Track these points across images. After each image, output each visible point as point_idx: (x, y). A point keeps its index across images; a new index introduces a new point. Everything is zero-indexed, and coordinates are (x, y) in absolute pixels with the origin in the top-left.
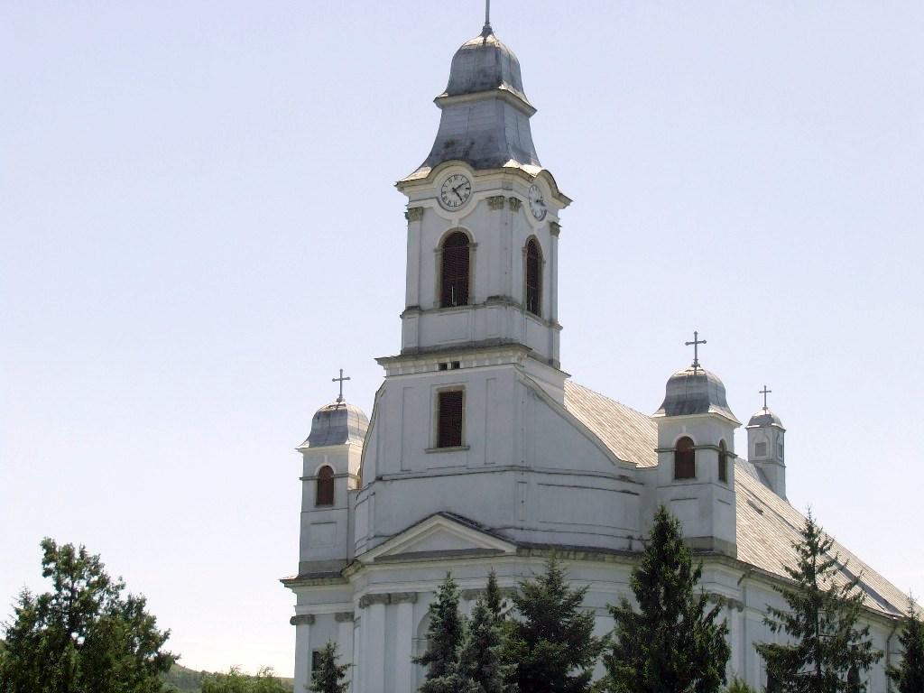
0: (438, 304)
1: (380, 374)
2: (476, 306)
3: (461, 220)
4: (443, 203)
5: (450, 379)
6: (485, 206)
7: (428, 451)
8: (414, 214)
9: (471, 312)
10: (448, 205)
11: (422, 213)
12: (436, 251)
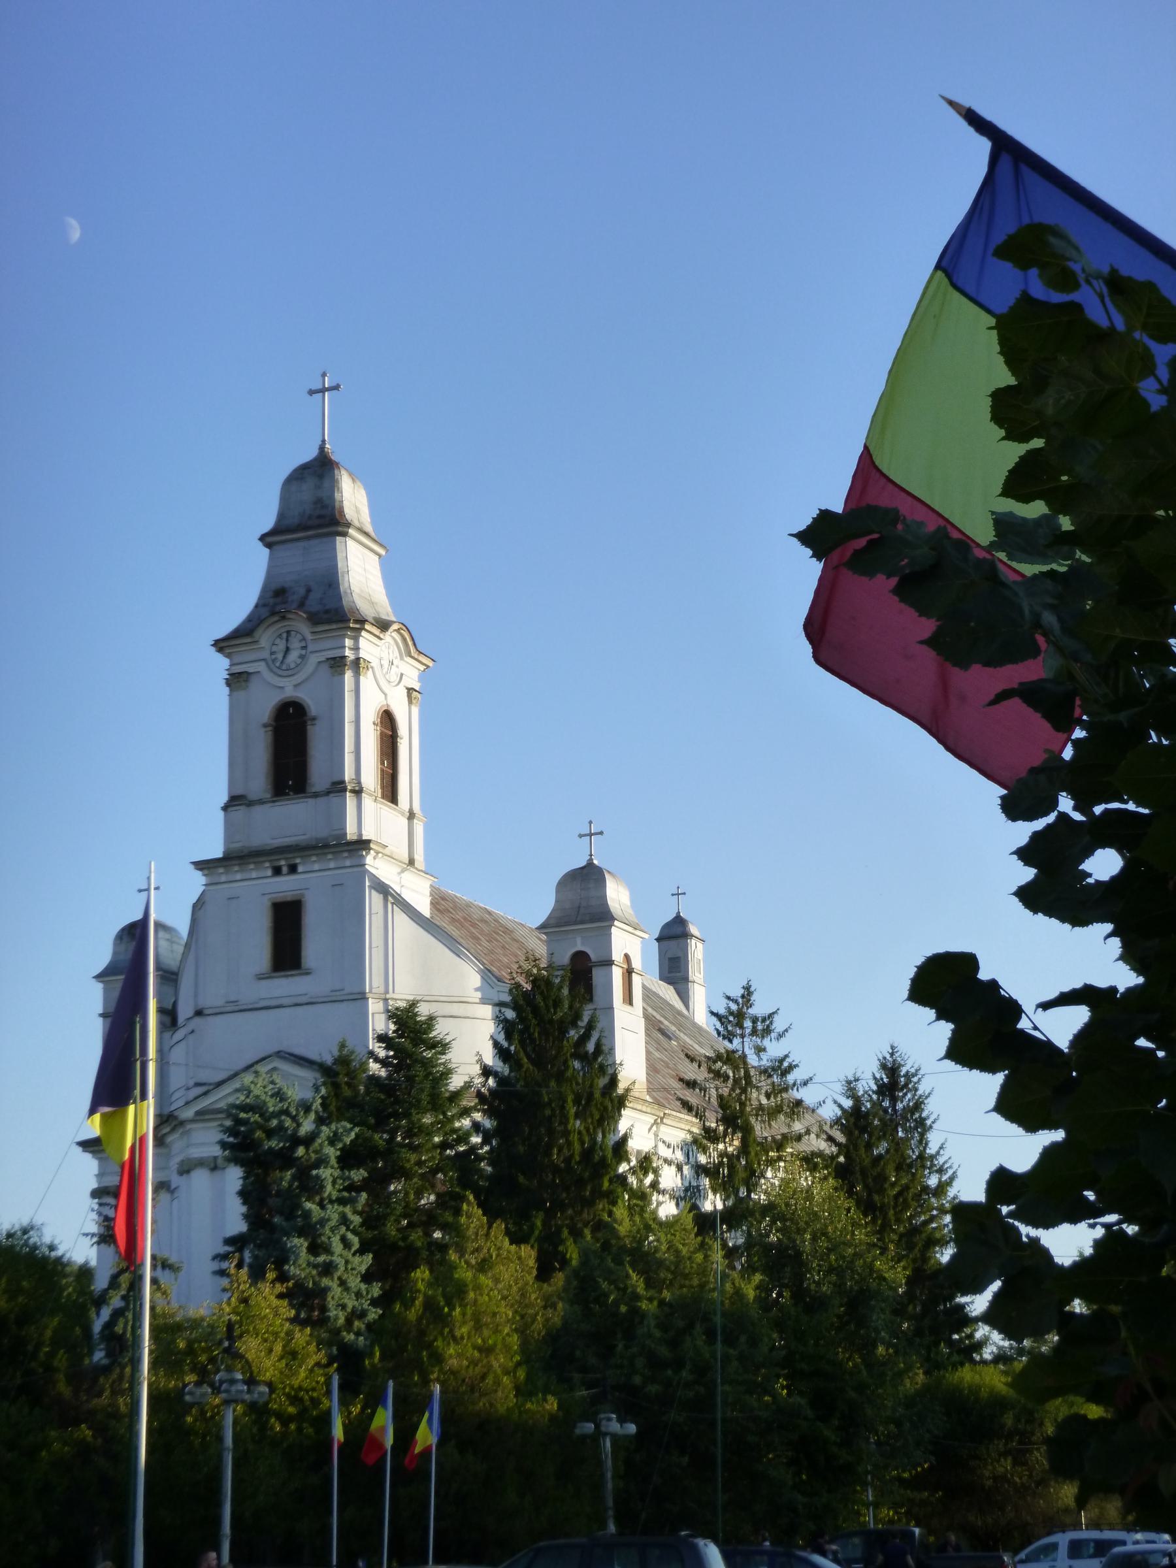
0: (268, 796)
1: (197, 882)
2: (316, 795)
3: (296, 686)
4: (272, 666)
5: (285, 886)
6: (325, 667)
7: (261, 977)
8: (236, 680)
9: (310, 800)
10: (279, 668)
11: (247, 681)
12: (265, 726)
